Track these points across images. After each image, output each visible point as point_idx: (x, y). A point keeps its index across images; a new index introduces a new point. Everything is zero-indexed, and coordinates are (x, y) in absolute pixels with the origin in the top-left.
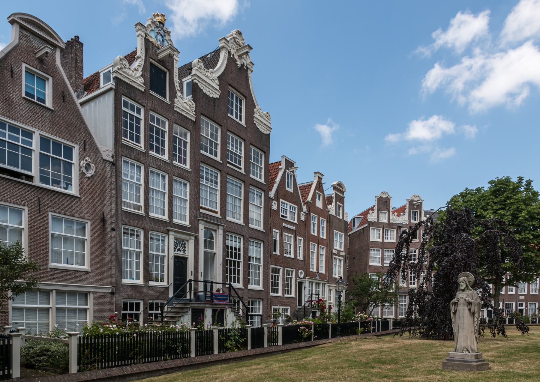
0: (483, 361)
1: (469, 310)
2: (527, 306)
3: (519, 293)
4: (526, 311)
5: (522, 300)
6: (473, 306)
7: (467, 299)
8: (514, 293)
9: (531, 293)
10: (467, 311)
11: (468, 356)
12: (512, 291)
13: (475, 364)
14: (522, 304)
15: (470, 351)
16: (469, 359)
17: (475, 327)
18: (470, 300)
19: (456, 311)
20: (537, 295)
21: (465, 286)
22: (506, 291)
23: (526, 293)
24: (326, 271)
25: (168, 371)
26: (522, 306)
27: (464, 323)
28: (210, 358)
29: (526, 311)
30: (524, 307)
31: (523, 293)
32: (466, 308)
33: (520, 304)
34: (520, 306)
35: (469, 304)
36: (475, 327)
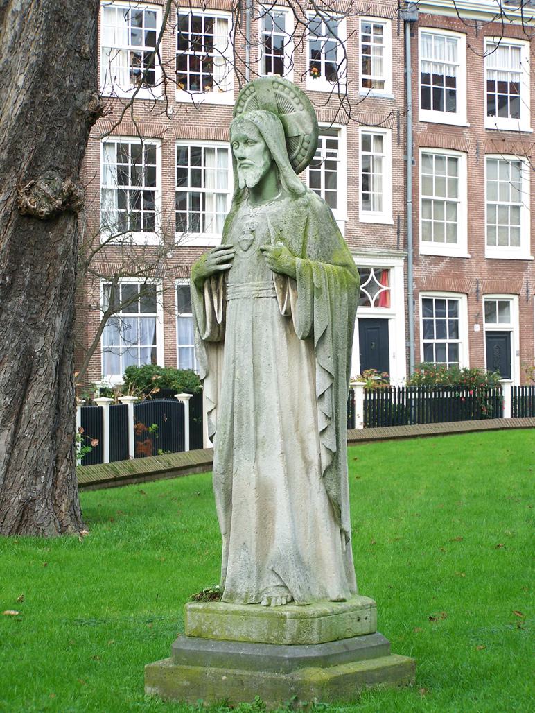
32: (272, 309)
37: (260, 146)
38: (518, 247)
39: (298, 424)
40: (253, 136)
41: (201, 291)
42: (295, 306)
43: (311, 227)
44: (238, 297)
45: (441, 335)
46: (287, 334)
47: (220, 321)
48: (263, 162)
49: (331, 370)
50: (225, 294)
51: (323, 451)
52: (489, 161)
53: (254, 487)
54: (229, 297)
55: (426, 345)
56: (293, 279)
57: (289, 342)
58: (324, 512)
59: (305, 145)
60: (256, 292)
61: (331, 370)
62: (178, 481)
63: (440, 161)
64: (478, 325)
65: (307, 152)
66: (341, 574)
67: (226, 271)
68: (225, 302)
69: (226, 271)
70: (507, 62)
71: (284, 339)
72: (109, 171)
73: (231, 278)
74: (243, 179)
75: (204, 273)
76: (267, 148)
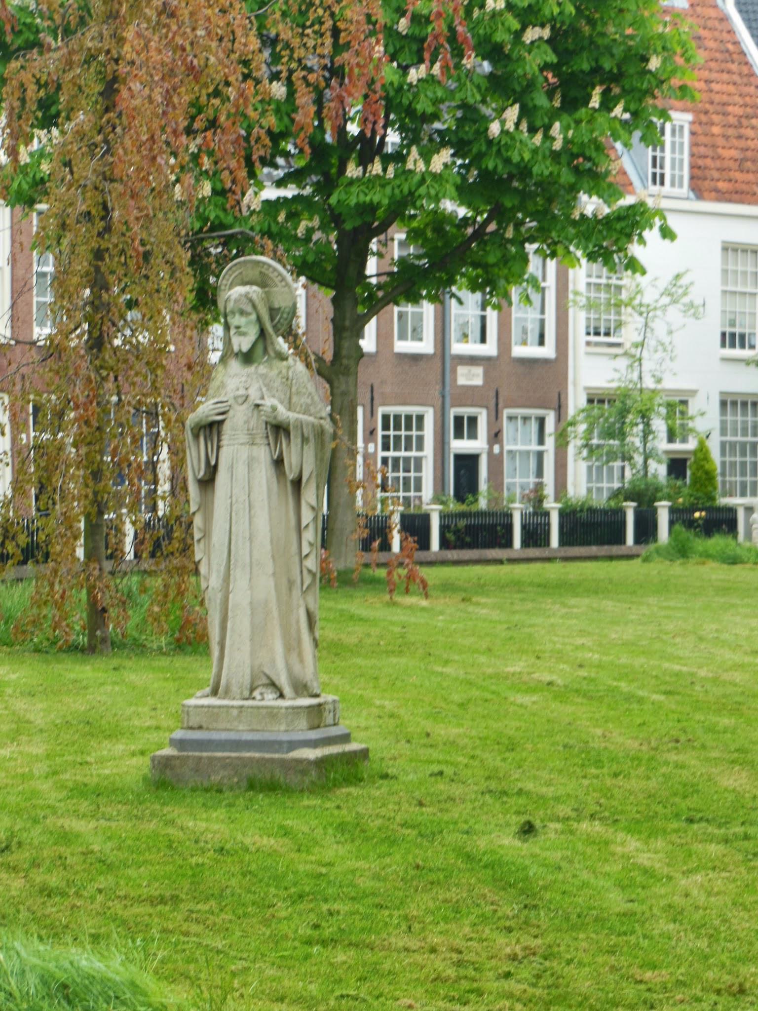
0: (345, 738)
1: (279, 463)
2: (495, 436)
3: (458, 348)
4: (496, 462)
5: (468, 395)
6: (296, 440)
7: (269, 402)
8: (426, 346)
9: (518, 351)
10: (264, 472)
11: (272, 714)
12: (417, 336)
13: (312, 754)
14: (473, 420)
15: (287, 690)
16: (280, 732)
17: (302, 558)
18: (284, 414)
19: (212, 471)
20: (545, 362)
21: (253, 333)
22: (384, 338)
23: (490, 349)
24: (463, 386)
25: (595, 558)
26: (473, 435)
27: (248, 535)
28: (545, 553)
29: (496, 462)
30: (477, 445)
31: (473, 348)
32: (263, 455)
33: (459, 420)
34: (459, 434)
35: (279, 430)
36: (302, 558)
37: (253, 317)
41: (196, 437)
45: (408, 448)
47: (213, 463)
49: (314, 503)
50: (219, 440)
52: (510, 418)
53: (271, 571)
54: (222, 443)
55: (384, 437)
56: (287, 433)
57: (279, 482)
58: (351, 596)
61: (314, 503)
64: (462, 370)
67: (222, 422)
68: (219, 448)
69: (222, 422)
70: (756, 8)
72: (370, 572)
73: (226, 427)
75: (203, 423)
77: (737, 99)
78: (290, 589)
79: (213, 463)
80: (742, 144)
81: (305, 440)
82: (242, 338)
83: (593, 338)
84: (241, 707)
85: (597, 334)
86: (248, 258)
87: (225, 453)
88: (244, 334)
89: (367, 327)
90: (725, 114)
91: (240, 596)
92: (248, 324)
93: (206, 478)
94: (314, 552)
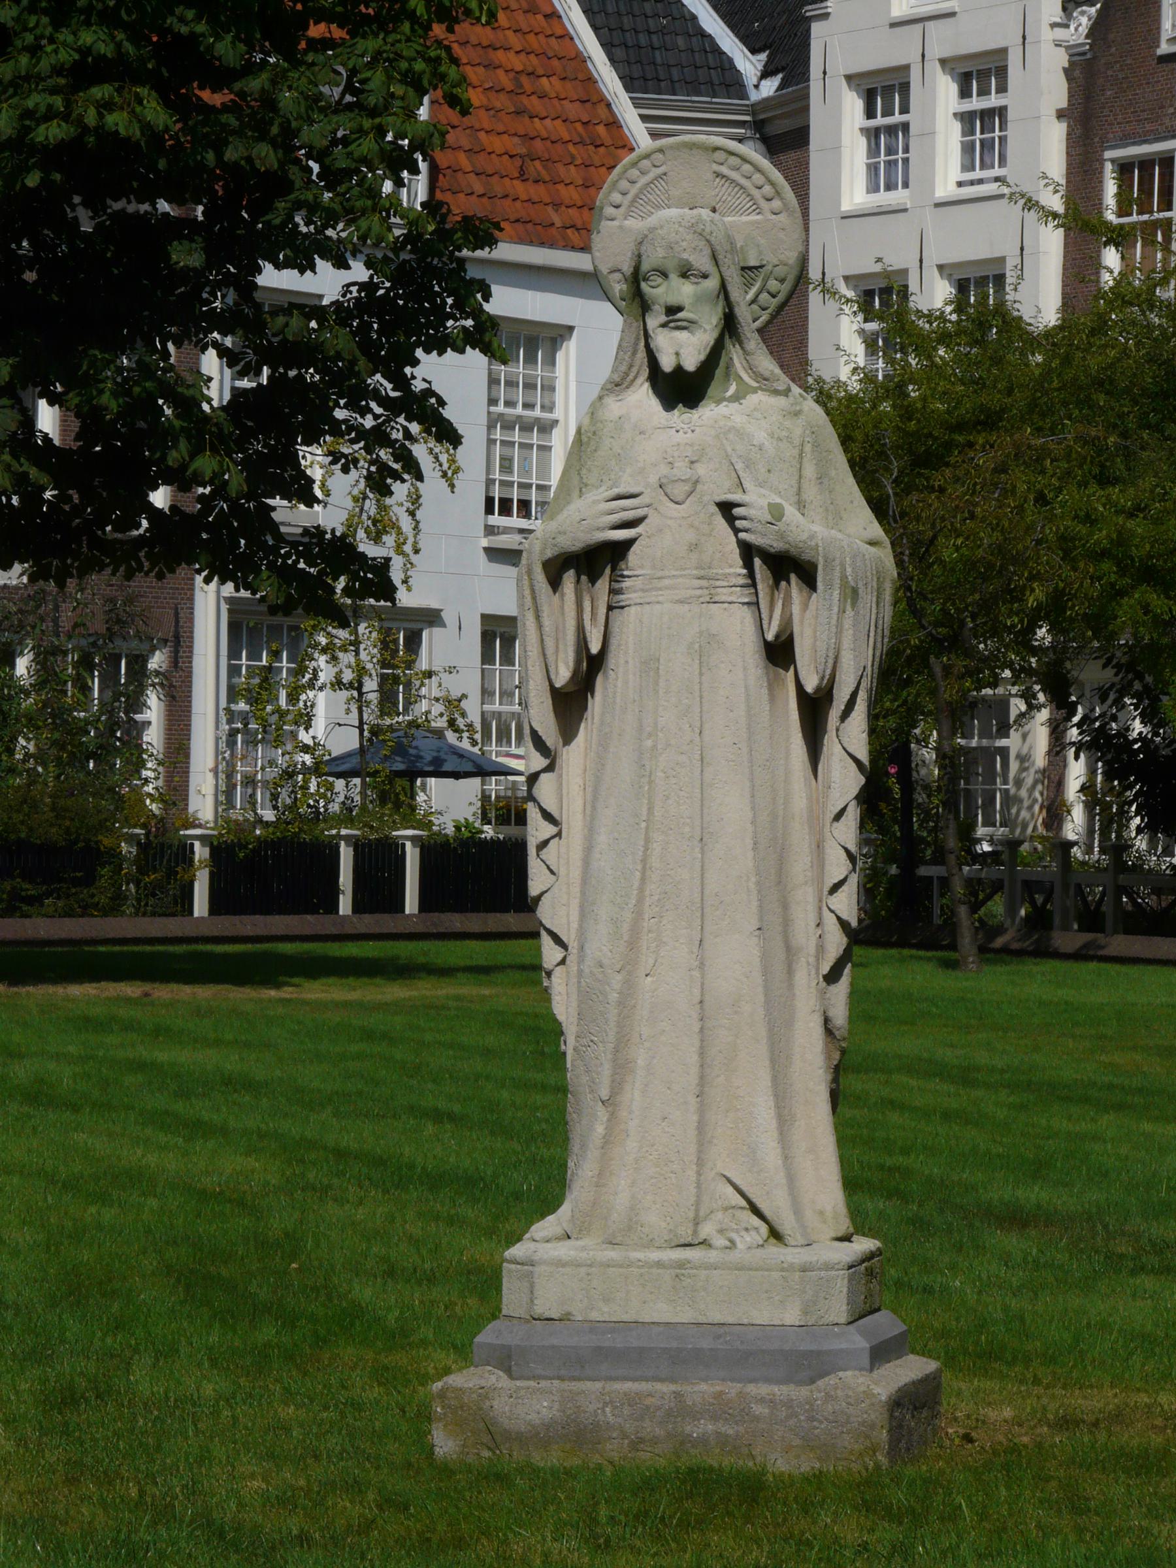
1: (779, 652)
19: (591, 666)
32: (737, 631)
37: (712, 284)
38: (489, 611)
39: (781, 869)
40: (702, 262)
41: (555, 583)
42: (802, 622)
43: (808, 456)
44: (661, 599)
46: (769, 680)
47: (595, 648)
48: (714, 321)
51: (831, 922)
59: (773, 285)
60: (706, 592)
62: (395, 992)
63: (524, 451)
65: (775, 302)
66: (607, 1142)
67: (628, 544)
69: (628, 544)
71: (765, 691)
74: (672, 351)
76: (723, 286)
77: (514, 40)
78: (790, 971)
79: (595, 648)
80: (523, 125)
81: (852, 594)
82: (683, 335)
83: (496, 520)
84: (681, 1264)
85: (505, 509)
86: (624, 162)
87: (628, 624)
88: (689, 326)
89: (717, 372)
90: (490, 66)
91: (666, 981)
92: (699, 299)
93: (572, 689)
94: (854, 880)
